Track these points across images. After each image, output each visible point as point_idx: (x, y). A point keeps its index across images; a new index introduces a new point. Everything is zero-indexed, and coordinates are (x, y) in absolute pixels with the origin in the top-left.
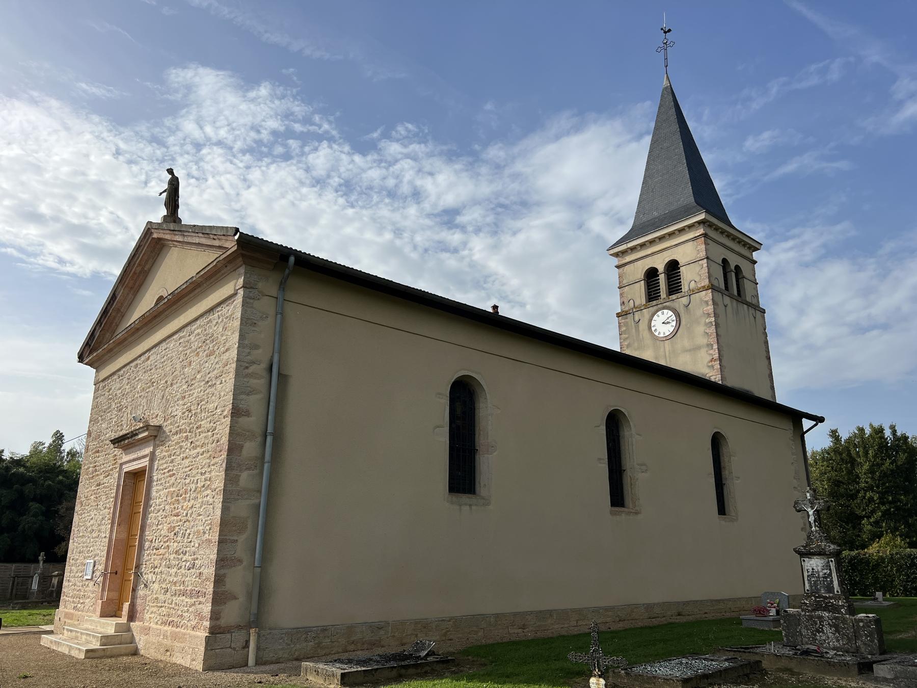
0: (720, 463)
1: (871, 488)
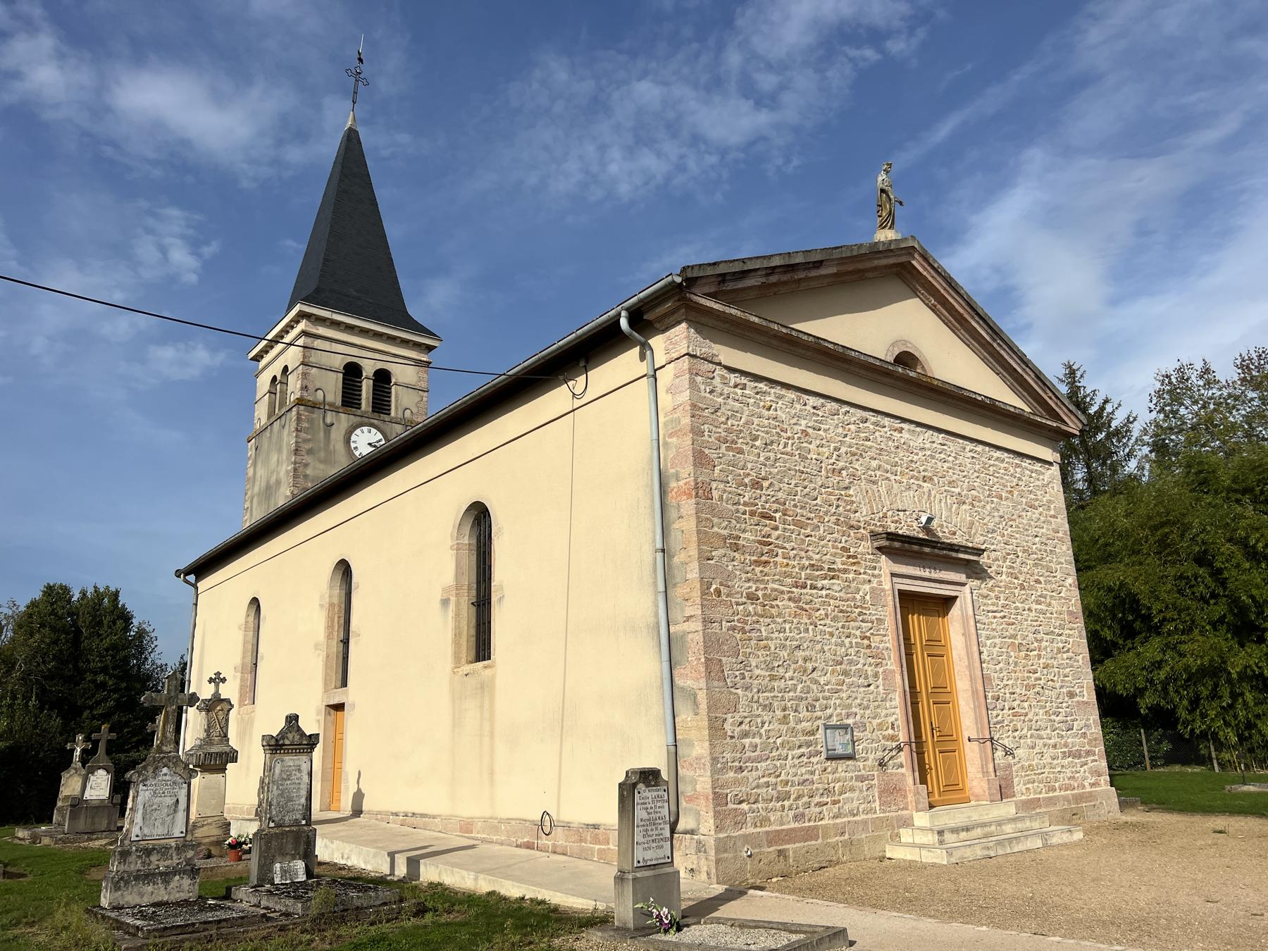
0: (478, 625)
1: (104, 670)
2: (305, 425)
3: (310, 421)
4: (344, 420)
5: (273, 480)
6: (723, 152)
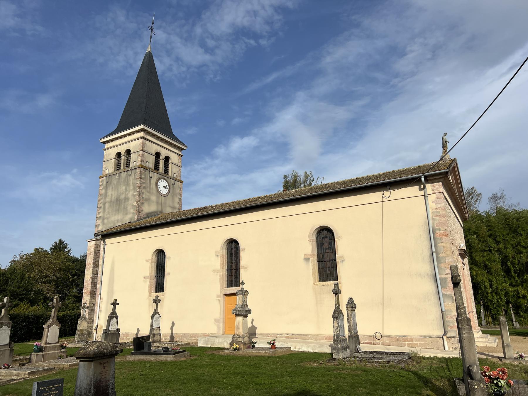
2: (143, 176)
3: (145, 175)
4: (155, 176)
5: (123, 197)
6: (189, 67)
